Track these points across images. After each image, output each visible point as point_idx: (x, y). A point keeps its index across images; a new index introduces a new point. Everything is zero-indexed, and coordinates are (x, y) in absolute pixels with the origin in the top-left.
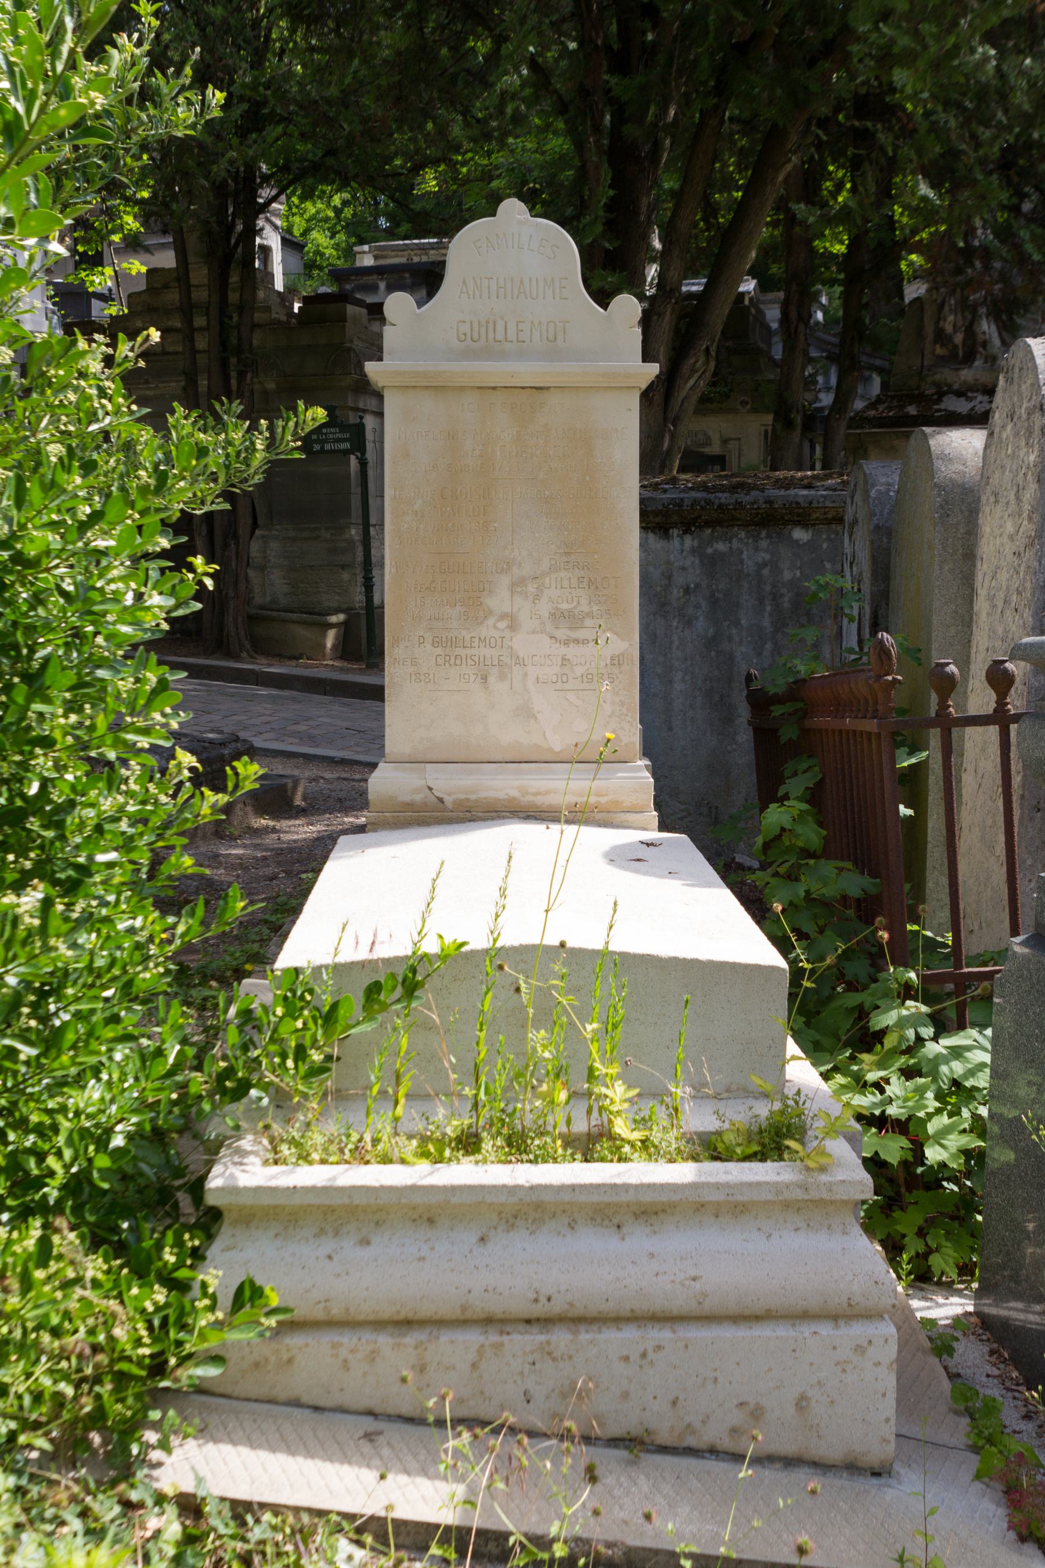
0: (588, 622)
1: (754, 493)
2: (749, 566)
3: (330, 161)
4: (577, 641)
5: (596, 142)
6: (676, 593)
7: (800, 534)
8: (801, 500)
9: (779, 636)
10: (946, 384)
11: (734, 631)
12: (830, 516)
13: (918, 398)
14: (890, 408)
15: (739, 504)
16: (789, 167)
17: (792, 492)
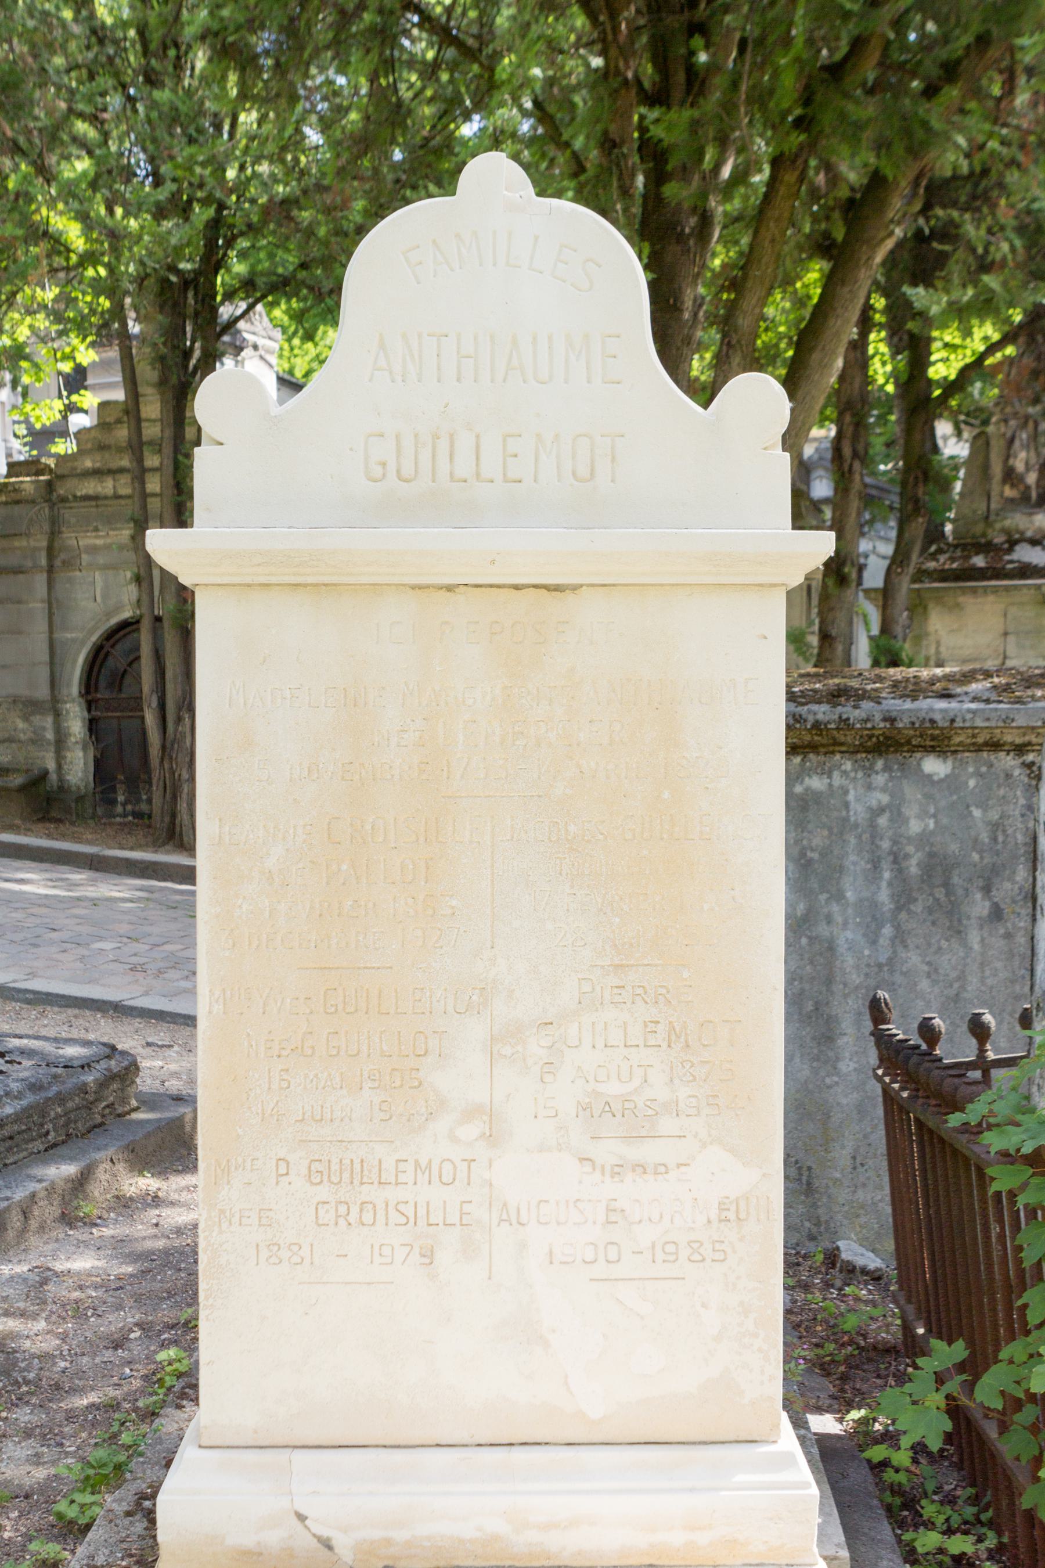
0: (667, 1125)
1: (866, 705)
2: (858, 811)
3: (302, 274)
4: (640, 1168)
5: (625, 210)
7: (934, 766)
8: (937, 717)
9: (903, 915)
10: (1018, 531)
11: (835, 908)
12: (980, 740)
13: (987, 548)
14: (953, 559)
15: (844, 723)
16: (890, 244)
17: (924, 704)
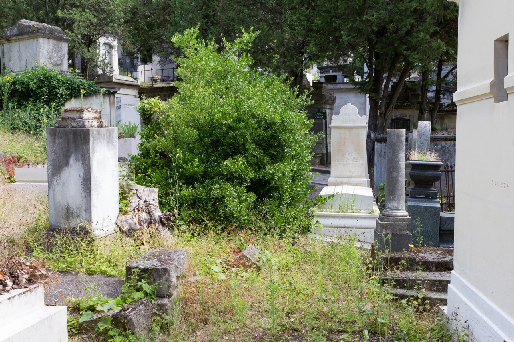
6: (383, 153)
